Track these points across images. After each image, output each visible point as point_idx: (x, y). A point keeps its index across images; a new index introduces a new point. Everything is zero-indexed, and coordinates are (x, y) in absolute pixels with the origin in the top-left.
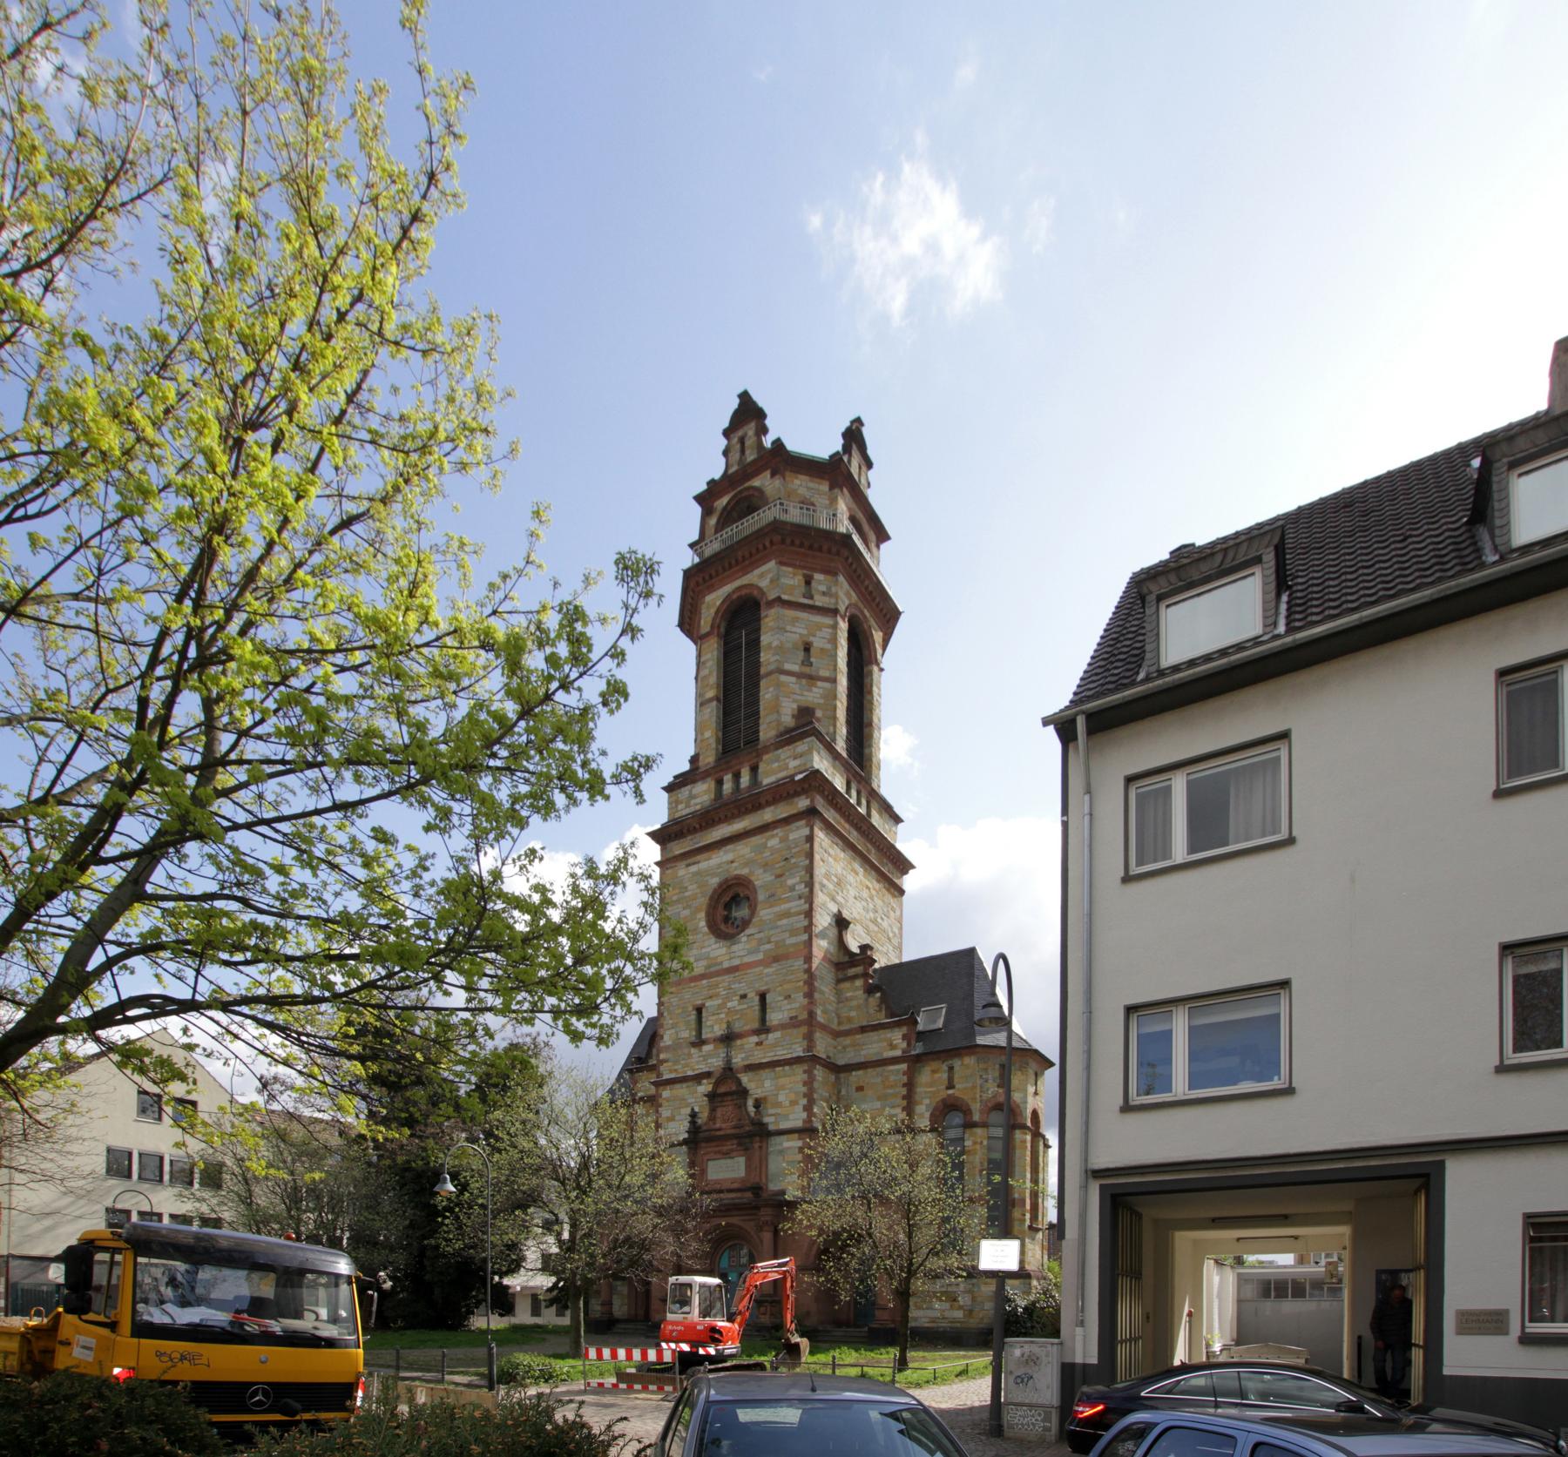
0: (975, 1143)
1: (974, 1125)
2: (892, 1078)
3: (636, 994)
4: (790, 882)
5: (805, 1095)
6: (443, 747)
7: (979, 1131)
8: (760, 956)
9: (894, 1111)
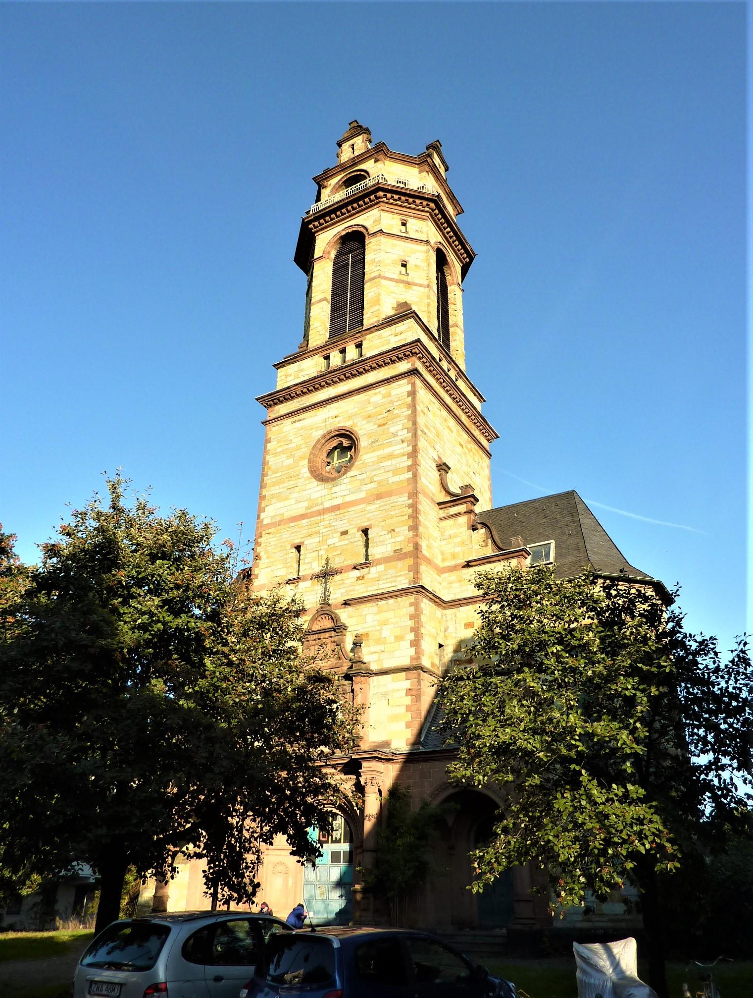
4: (393, 430)
8: (363, 495)
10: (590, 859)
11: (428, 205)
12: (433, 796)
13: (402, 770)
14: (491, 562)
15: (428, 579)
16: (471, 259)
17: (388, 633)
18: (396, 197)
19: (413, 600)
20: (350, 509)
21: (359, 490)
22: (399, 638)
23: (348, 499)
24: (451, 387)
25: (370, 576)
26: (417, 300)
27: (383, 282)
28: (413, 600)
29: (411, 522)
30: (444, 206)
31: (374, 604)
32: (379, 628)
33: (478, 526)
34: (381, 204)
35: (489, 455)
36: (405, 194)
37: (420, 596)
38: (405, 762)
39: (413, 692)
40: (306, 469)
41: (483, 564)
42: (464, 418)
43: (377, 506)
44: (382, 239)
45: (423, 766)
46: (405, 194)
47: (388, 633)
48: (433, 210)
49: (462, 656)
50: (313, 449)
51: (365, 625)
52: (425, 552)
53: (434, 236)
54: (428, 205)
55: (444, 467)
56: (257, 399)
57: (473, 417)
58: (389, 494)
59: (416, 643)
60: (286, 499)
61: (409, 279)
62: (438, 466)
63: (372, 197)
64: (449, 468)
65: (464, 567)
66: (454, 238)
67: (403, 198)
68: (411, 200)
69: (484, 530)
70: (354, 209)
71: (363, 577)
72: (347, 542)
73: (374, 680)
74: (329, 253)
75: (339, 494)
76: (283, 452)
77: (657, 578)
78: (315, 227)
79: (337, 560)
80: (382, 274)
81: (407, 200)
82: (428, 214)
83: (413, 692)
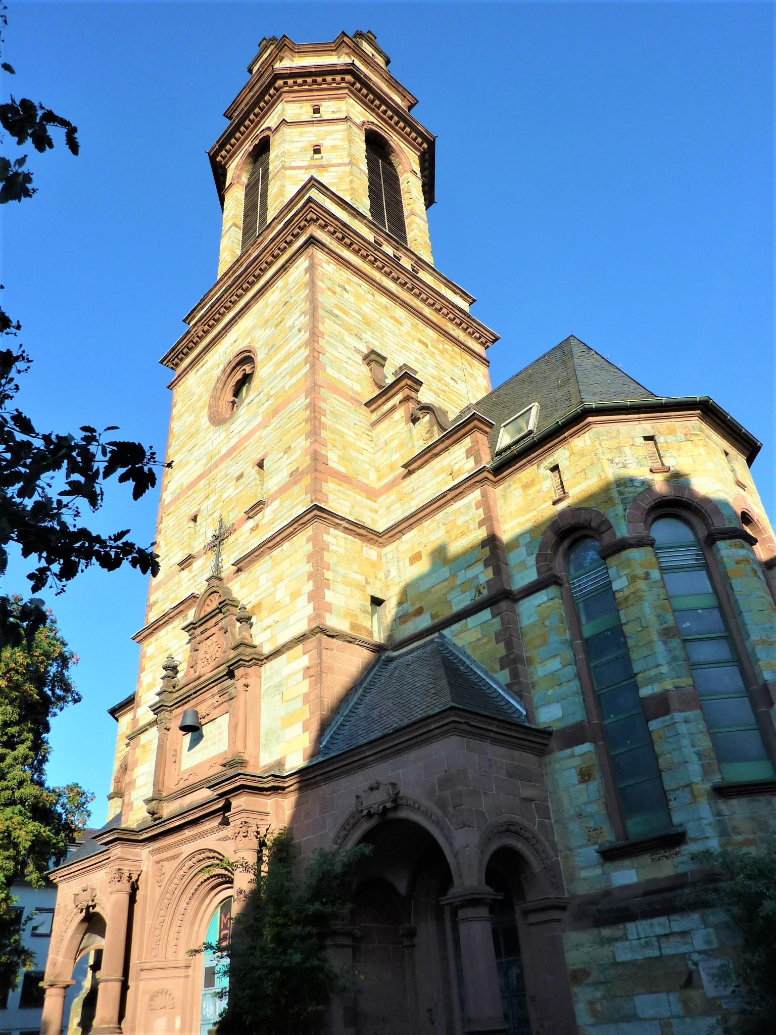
0: (633, 579)
1: (623, 545)
2: (460, 521)
3: (50, 434)
4: (289, 323)
5: (310, 576)
6: (53, 670)
7: (635, 554)
8: (259, 419)
9: (471, 573)
10: (31, 867)
11: (343, 79)
12: (341, 839)
13: (298, 804)
14: (437, 455)
15: (339, 501)
16: (432, 144)
17: (282, 594)
18: (300, 81)
19: (311, 533)
20: (246, 444)
21: (255, 415)
22: (295, 595)
23: (245, 432)
24: (411, 282)
25: (265, 521)
26: (336, 180)
27: (288, 172)
28: (311, 533)
29: (308, 427)
30: (365, 75)
31: (267, 558)
32: (272, 589)
33: (419, 414)
34: (284, 95)
35: (486, 362)
36: (309, 74)
37: (317, 524)
38: (300, 789)
39: (312, 671)
40: (206, 419)
41: (427, 462)
42: (427, 311)
43: (274, 425)
44: (285, 130)
45: (325, 789)
46: (309, 74)
47: (282, 594)
48: (353, 85)
49: (409, 607)
50: (213, 392)
51: (257, 592)
52: (333, 459)
53: (359, 113)
54: (343, 79)
55: (373, 357)
56: (162, 362)
57: (444, 311)
58: (286, 403)
59: (316, 596)
60: (188, 463)
61: (324, 162)
62: (365, 358)
63: (272, 91)
64: (385, 359)
65: (405, 476)
66: (396, 118)
67: (309, 80)
68: (319, 79)
69: (428, 417)
70: (256, 115)
71: (257, 526)
72: (242, 487)
73: (268, 668)
74: (239, 177)
75: (236, 432)
76: (186, 411)
77: (698, 395)
78: (224, 158)
79: (232, 515)
80: (287, 165)
81: (314, 81)
82: (346, 91)
83: (312, 671)
